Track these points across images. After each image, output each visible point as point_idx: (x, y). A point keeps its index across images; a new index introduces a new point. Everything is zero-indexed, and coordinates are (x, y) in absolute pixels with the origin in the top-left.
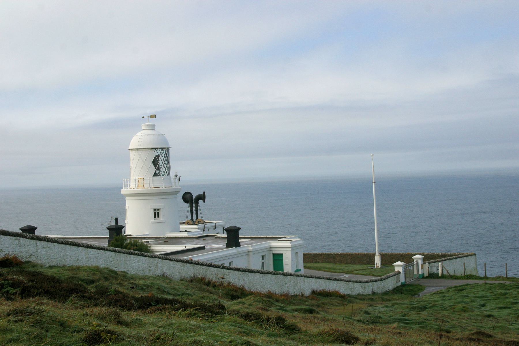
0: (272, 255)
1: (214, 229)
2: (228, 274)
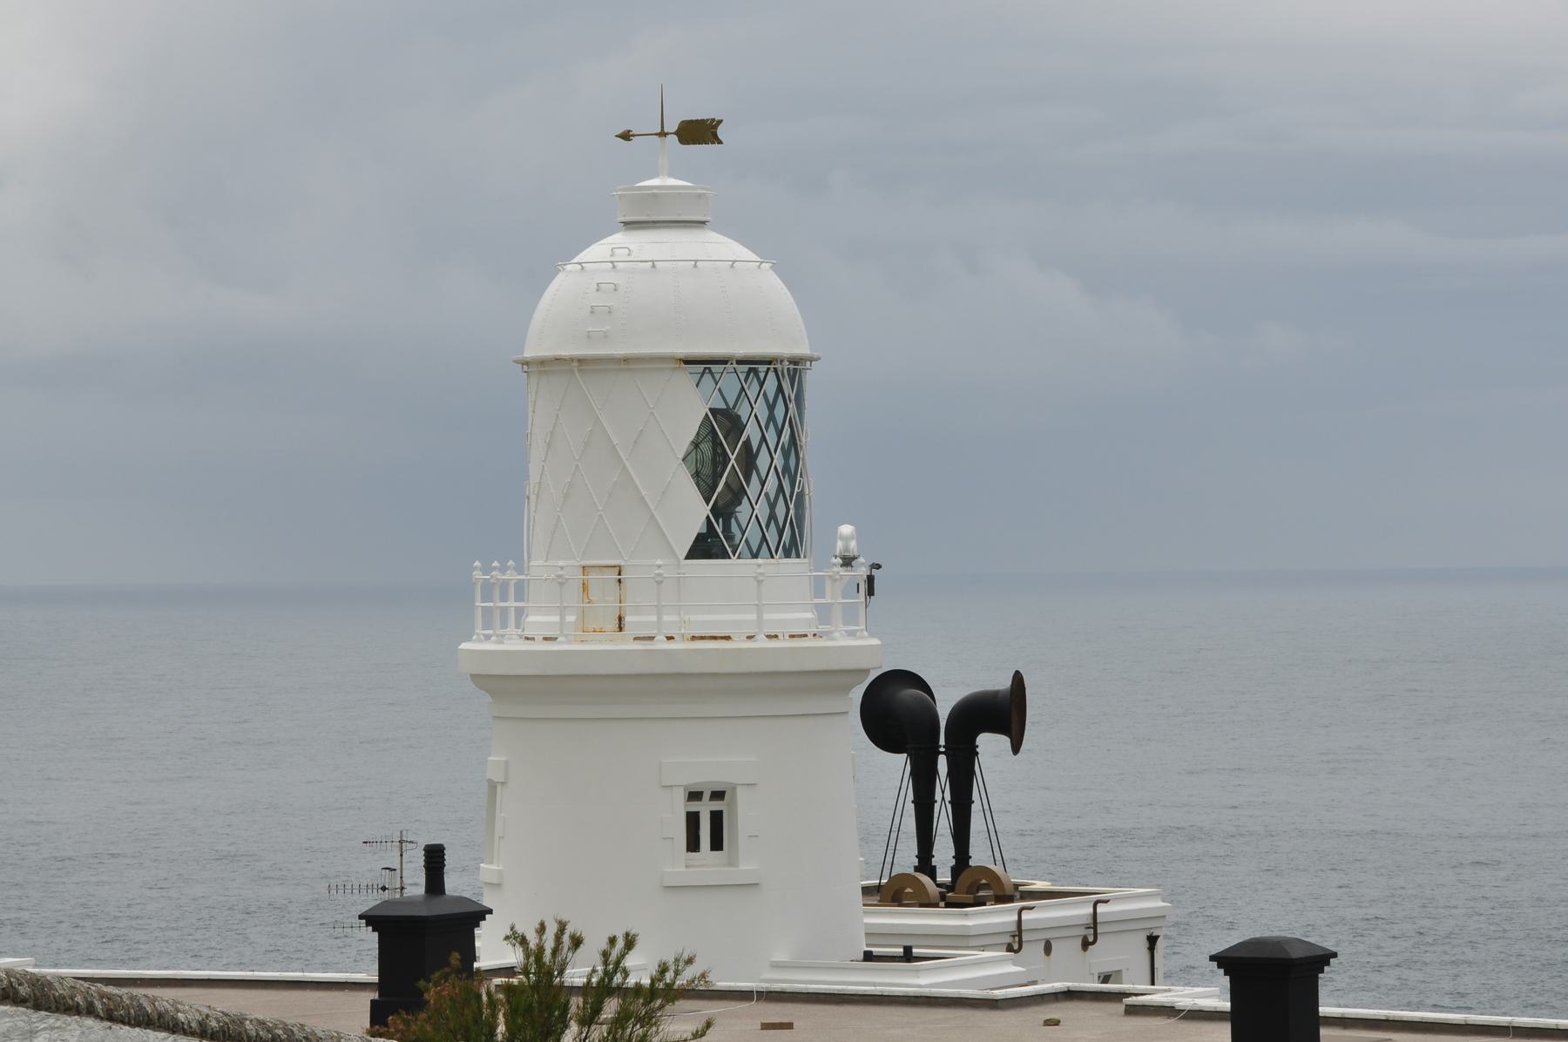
1: (1086, 944)
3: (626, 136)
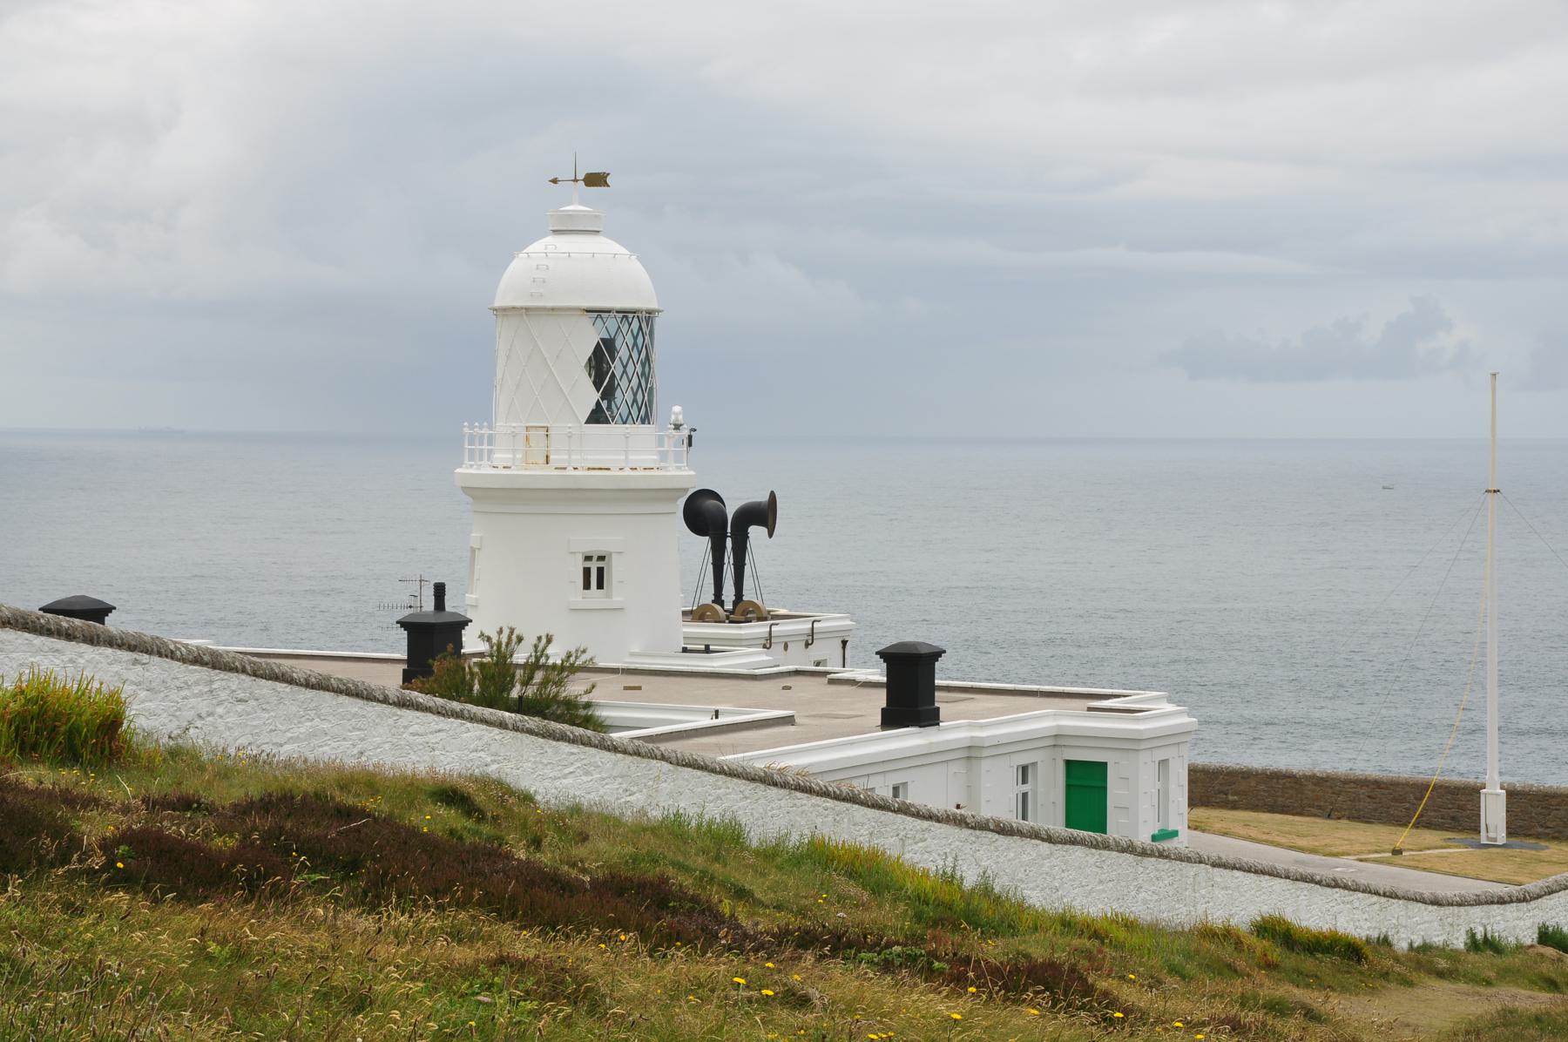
1: (807, 645)
2: (919, 836)
3: (555, 181)
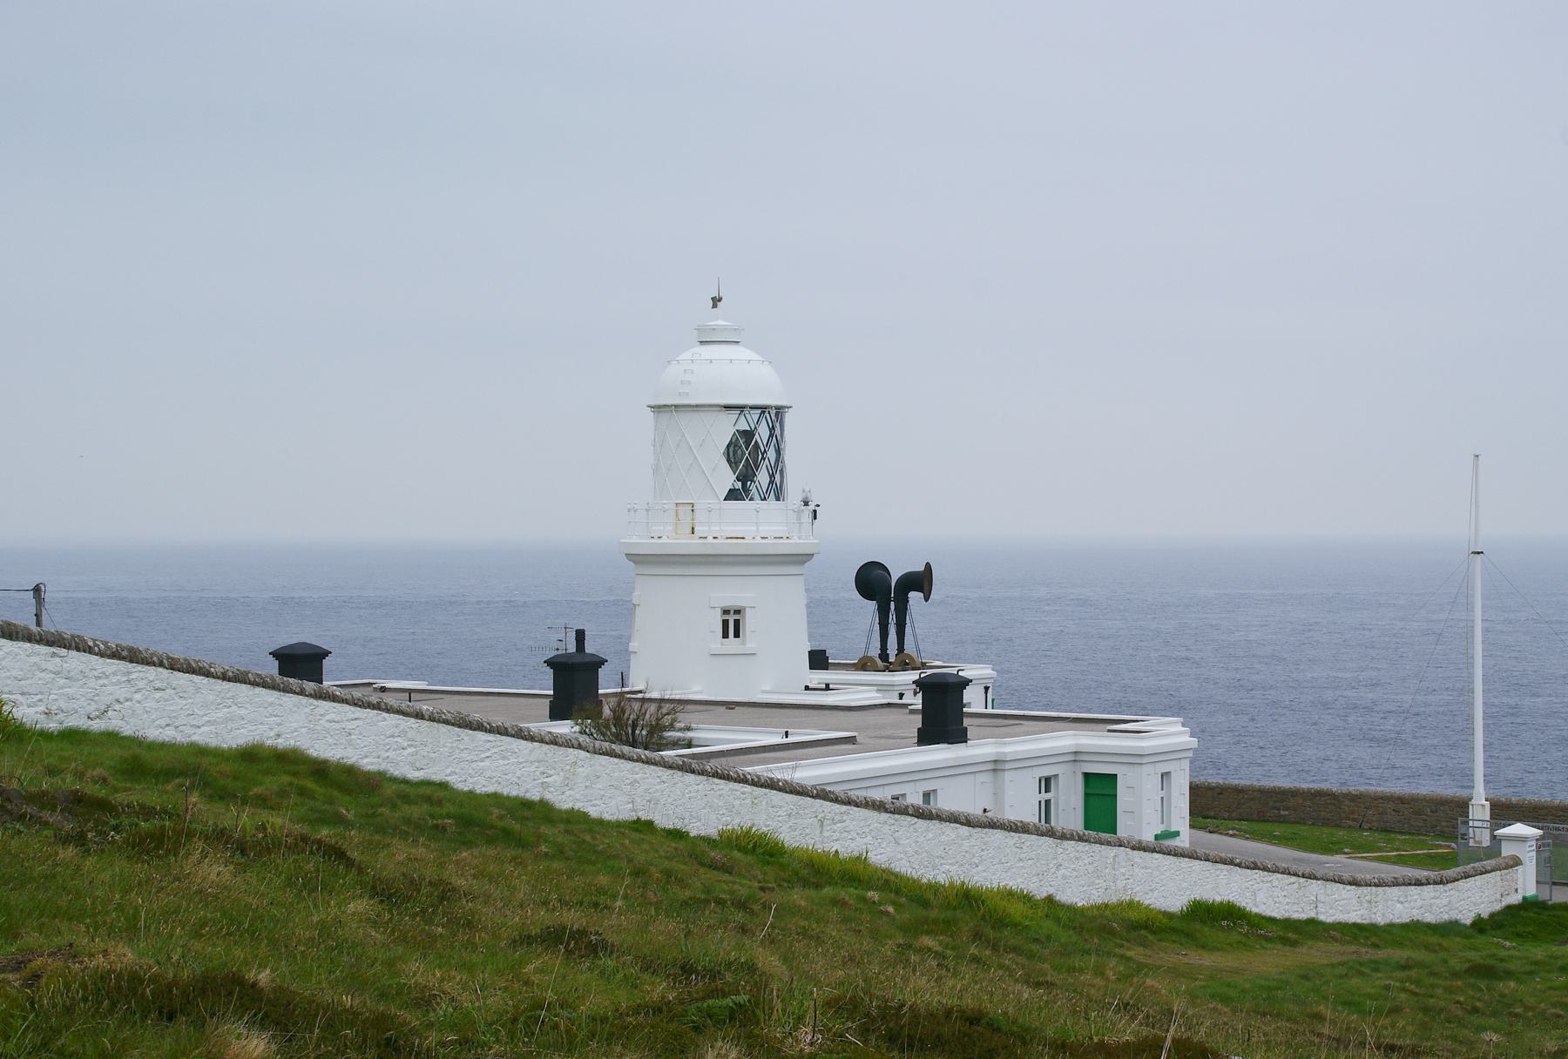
0: (1080, 779)
2: (837, 818)
3: (716, 301)
